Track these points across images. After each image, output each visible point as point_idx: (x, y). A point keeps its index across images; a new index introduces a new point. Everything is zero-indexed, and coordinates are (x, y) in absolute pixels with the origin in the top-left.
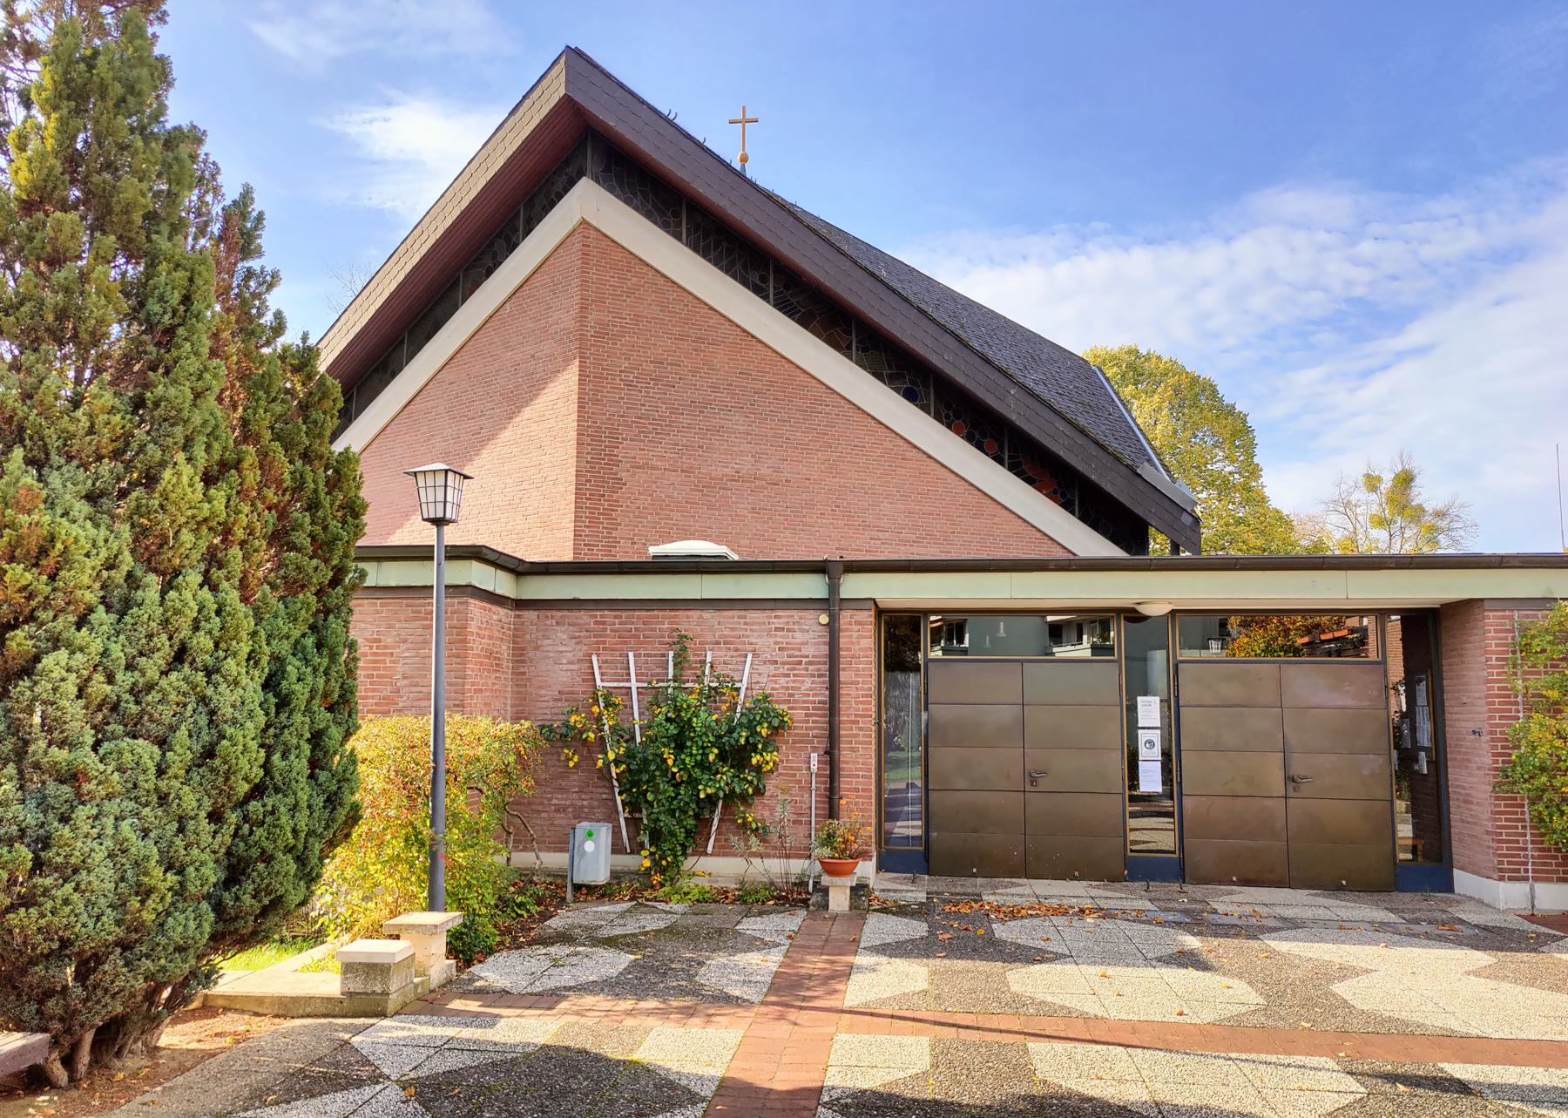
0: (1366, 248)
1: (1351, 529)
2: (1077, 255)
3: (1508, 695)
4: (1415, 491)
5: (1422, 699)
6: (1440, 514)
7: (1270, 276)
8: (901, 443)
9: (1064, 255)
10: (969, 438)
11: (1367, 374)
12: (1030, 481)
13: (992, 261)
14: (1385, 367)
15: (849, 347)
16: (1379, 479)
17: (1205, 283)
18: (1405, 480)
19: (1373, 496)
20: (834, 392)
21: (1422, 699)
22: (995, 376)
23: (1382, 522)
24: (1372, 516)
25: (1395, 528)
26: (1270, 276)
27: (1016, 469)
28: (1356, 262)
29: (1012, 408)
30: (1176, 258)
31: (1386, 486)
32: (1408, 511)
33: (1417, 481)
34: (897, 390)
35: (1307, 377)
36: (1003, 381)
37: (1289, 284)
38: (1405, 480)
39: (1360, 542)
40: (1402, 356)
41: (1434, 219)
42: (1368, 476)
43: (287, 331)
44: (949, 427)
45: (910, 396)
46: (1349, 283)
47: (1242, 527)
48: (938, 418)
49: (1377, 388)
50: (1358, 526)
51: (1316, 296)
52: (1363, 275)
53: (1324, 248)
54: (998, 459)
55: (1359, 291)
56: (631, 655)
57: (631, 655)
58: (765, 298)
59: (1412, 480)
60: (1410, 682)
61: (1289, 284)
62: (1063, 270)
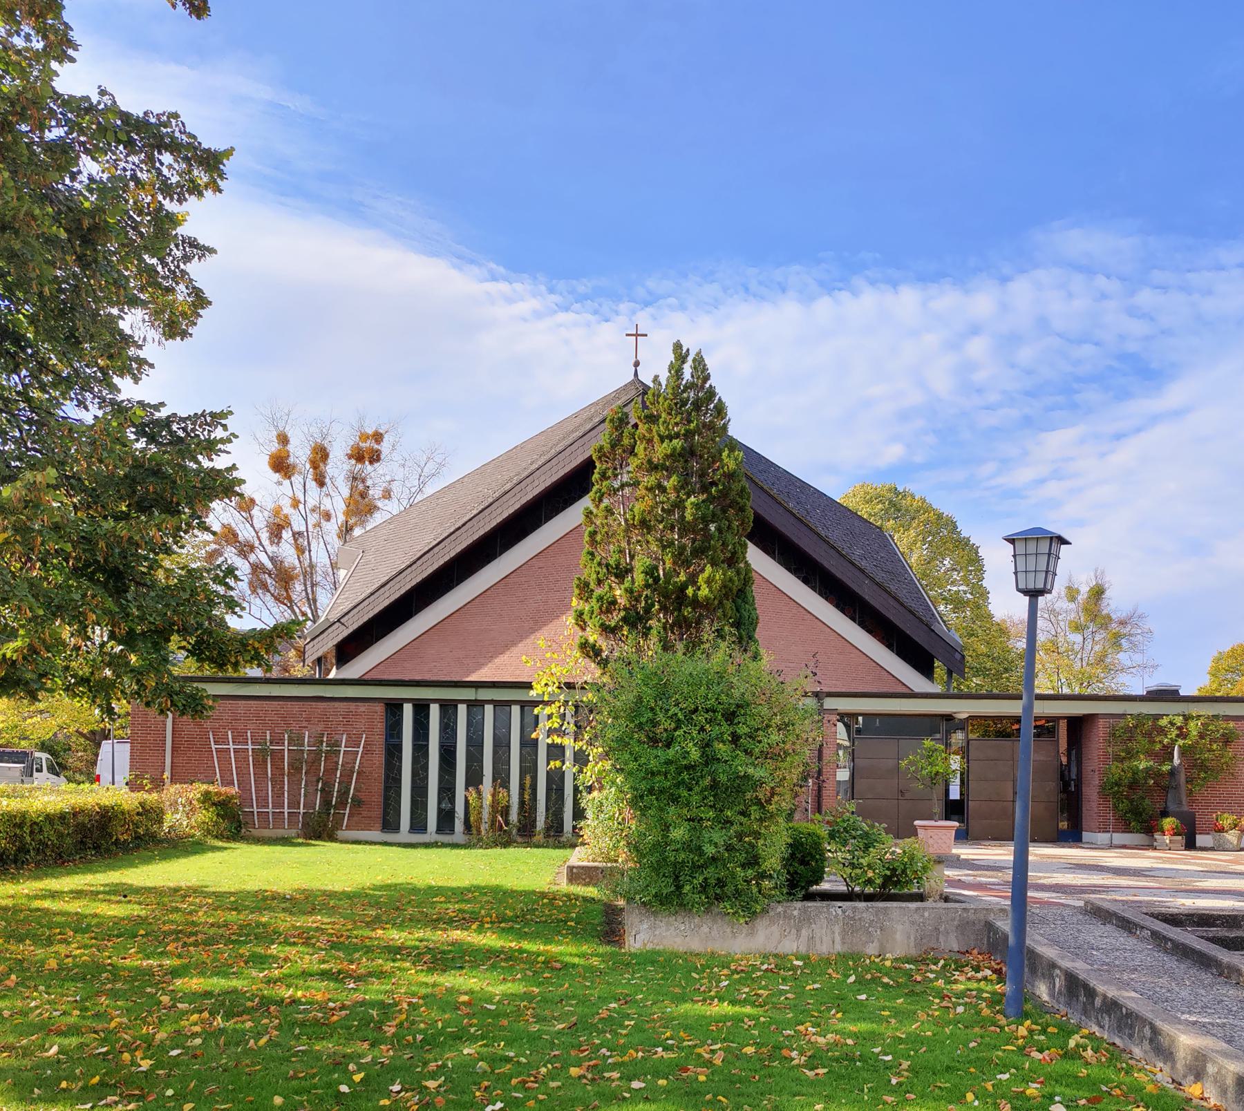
0: (1145, 298)
1: (1054, 633)
2: (840, 290)
3: (1106, 754)
4: (1104, 603)
5: (1073, 758)
6: (1123, 623)
7: (1043, 324)
8: (802, 610)
9: (829, 287)
10: (837, 606)
11: (1119, 437)
12: (869, 631)
13: (747, 290)
14: (1138, 430)
15: (774, 553)
16: (1078, 591)
17: (975, 330)
18: (1098, 593)
19: (1072, 606)
20: (767, 580)
21: (1073, 758)
22: (858, 573)
23: (1078, 628)
24: (1071, 622)
25: (1087, 633)
26: (1043, 324)
27: (862, 625)
28: (1133, 312)
29: (866, 592)
30: (947, 299)
31: (1082, 597)
32: (1098, 620)
33: (1107, 594)
34: (798, 577)
35: (1058, 441)
36: (861, 576)
37: (1059, 335)
38: (1098, 593)
39: (1060, 645)
40: (1154, 419)
41: (1220, 268)
42: (1069, 588)
43: (271, 471)
44: (826, 599)
45: (806, 581)
46: (1122, 338)
47: (973, 639)
48: (821, 594)
49: (1125, 455)
50: (1059, 629)
51: (1087, 350)
52: (1138, 328)
53: (1104, 296)
54: (853, 619)
55: (1132, 347)
56: (230, 733)
57: (230, 733)
58: (855, 622)
59: (1103, 592)
60: (1069, 750)
61: (1059, 335)
62: (824, 307)
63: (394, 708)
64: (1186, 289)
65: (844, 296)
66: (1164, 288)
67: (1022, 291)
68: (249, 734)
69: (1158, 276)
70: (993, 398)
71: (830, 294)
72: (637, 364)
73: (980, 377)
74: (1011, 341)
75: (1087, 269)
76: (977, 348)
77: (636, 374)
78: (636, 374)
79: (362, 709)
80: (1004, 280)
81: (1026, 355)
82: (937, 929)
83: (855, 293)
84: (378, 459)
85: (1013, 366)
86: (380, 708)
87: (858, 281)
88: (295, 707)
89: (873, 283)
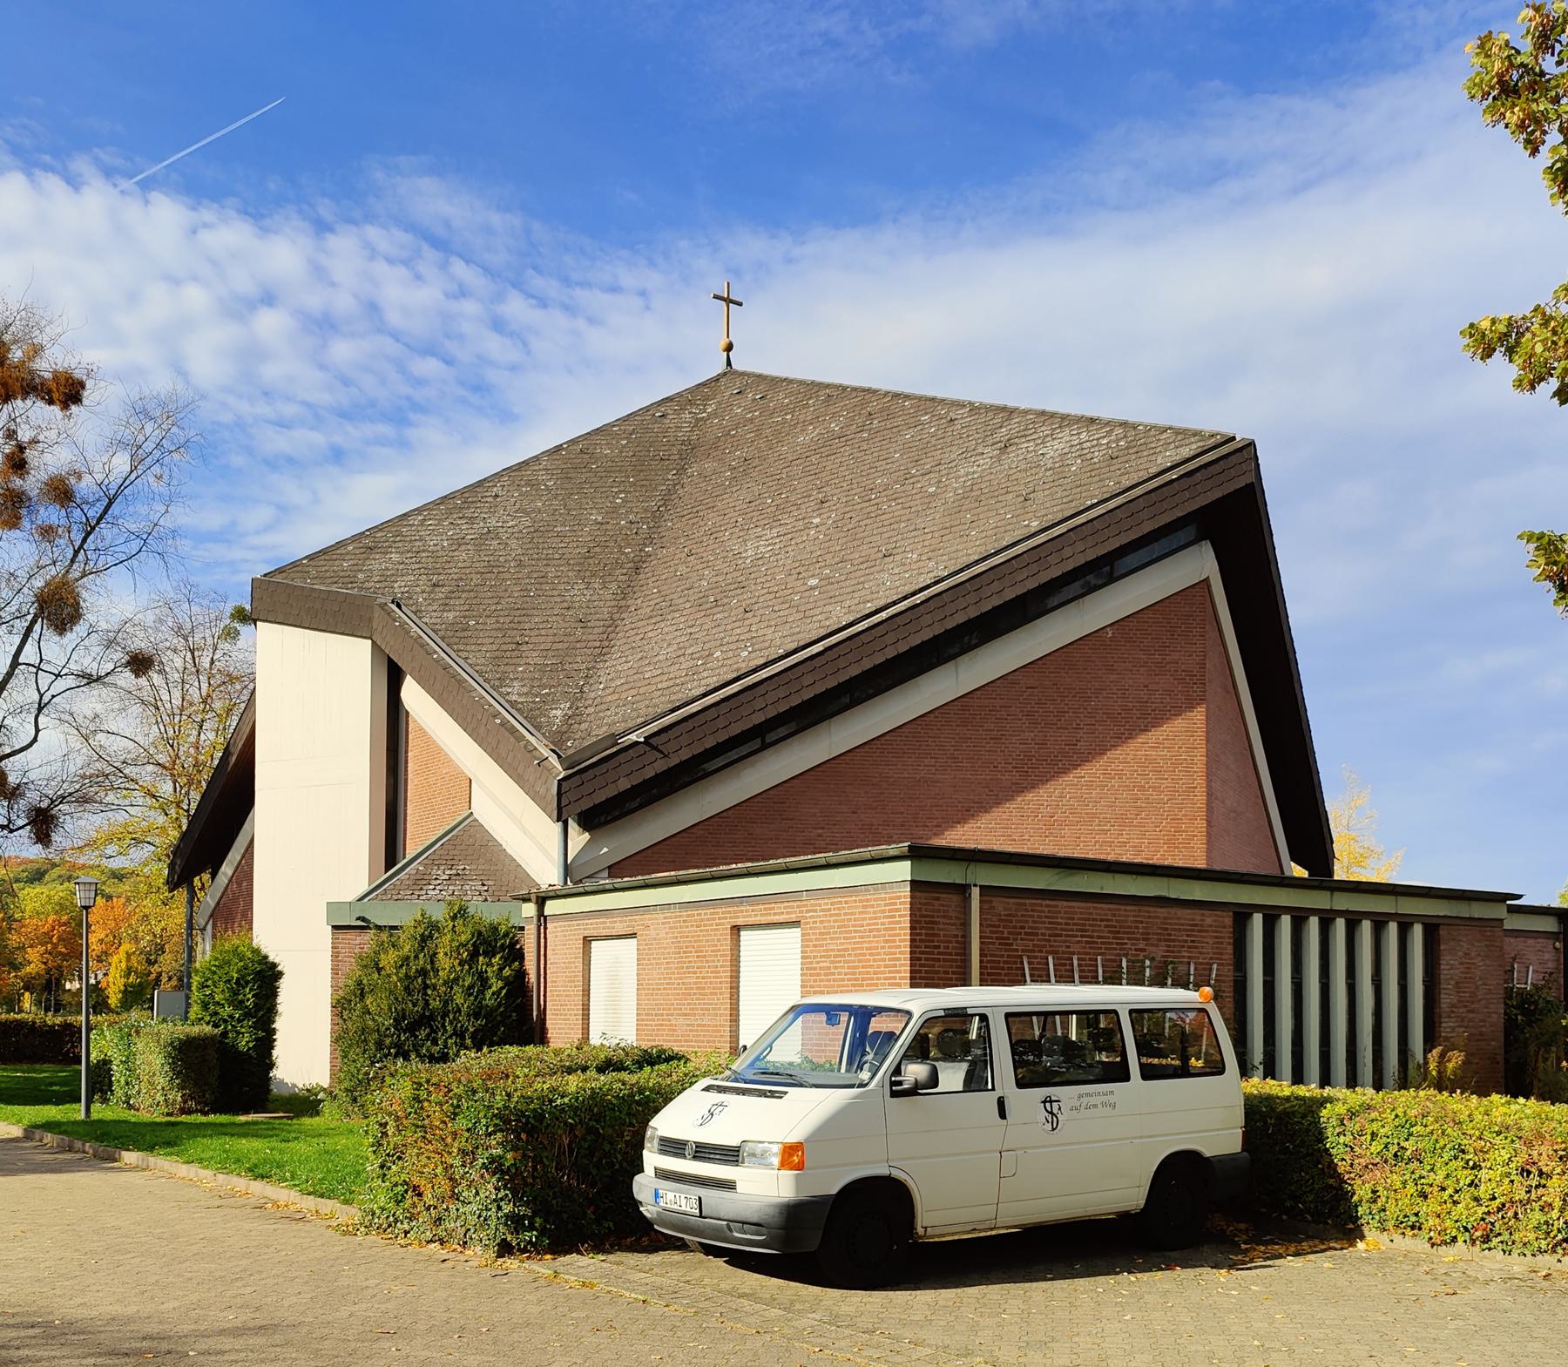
17: (268, 299)
41: (614, 289)
53: (462, 293)
56: (1050, 959)
63: (1242, 915)
64: (569, 309)
65: (53, 183)
66: (543, 303)
67: (344, 249)
68: (1075, 962)
69: (538, 282)
70: (289, 410)
71: (29, 175)
72: (729, 348)
73: (271, 372)
74: (323, 325)
75: (442, 243)
76: (270, 324)
77: (729, 363)
78: (729, 363)
79: (1209, 921)
80: (322, 228)
81: (342, 351)
82: (417, 1099)
83: (74, 183)
84: (76, 399)
85: (322, 367)
86: (1227, 919)
87: (81, 165)
88: (1129, 913)
89: (109, 173)
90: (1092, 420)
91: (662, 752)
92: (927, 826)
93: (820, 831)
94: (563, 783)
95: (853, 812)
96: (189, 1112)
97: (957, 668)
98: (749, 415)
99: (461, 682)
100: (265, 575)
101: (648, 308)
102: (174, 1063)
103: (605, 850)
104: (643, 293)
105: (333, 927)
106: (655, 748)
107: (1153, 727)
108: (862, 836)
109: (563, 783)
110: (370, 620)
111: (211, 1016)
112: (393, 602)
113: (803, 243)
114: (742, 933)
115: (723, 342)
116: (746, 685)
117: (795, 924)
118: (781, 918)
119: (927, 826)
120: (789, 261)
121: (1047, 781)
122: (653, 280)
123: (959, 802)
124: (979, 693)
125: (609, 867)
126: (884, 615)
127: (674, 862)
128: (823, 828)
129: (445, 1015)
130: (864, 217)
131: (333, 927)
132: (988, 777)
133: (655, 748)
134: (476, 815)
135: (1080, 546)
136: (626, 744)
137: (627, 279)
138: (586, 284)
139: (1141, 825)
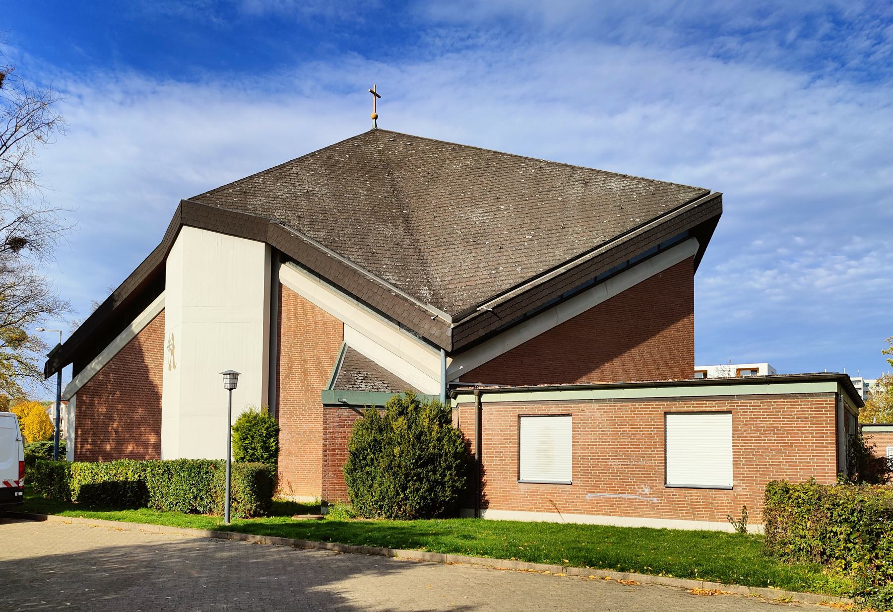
41: (65, 92)
72: (376, 118)
90: (624, 176)
91: (499, 317)
92: (593, 362)
93: (551, 362)
94: (454, 330)
95: (565, 354)
96: (260, 516)
97: (606, 285)
98: (410, 152)
99: (355, 271)
100: (189, 199)
101: (82, 104)
102: (252, 486)
103: (462, 367)
104: (80, 97)
105: (324, 404)
106: (495, 315)
107: (676, 321)
108: (568, 365)
109: (454, 330)
110: (266, 232)
111: (251, 456)
112: (281, 224)
113: (163, 85)
114: (667, 416)
115: (373, 115)
116: (534, 286)
117: (729, 412)
118: (713, 409)
119: (593, 362)
120: (154, 92)
121: (639, 343)
122: (86, 91)
123: (606, 352)
124: (613, 299)
125: (460, 377)
126: (588, 257)
127: (489, 375)
128: (552, 361)
129: (441, 456)
130: (194, 80)
131: (324, 404)
132: (617, 340)
133: (495, 315)
134: (349, 345)
135: (663, 233)
136: (482, 311)
137: (72, 88)
138: (51, 88)
139: (672, 367)
